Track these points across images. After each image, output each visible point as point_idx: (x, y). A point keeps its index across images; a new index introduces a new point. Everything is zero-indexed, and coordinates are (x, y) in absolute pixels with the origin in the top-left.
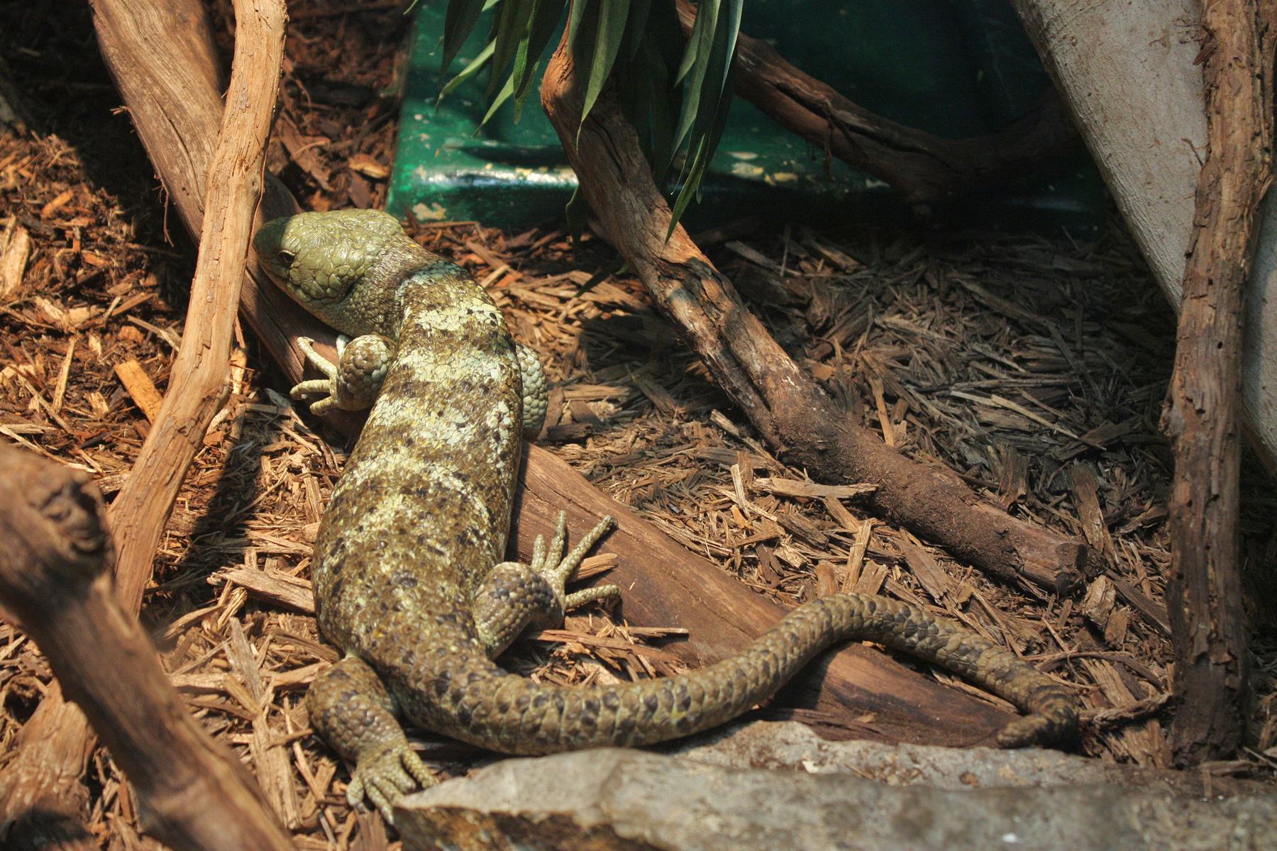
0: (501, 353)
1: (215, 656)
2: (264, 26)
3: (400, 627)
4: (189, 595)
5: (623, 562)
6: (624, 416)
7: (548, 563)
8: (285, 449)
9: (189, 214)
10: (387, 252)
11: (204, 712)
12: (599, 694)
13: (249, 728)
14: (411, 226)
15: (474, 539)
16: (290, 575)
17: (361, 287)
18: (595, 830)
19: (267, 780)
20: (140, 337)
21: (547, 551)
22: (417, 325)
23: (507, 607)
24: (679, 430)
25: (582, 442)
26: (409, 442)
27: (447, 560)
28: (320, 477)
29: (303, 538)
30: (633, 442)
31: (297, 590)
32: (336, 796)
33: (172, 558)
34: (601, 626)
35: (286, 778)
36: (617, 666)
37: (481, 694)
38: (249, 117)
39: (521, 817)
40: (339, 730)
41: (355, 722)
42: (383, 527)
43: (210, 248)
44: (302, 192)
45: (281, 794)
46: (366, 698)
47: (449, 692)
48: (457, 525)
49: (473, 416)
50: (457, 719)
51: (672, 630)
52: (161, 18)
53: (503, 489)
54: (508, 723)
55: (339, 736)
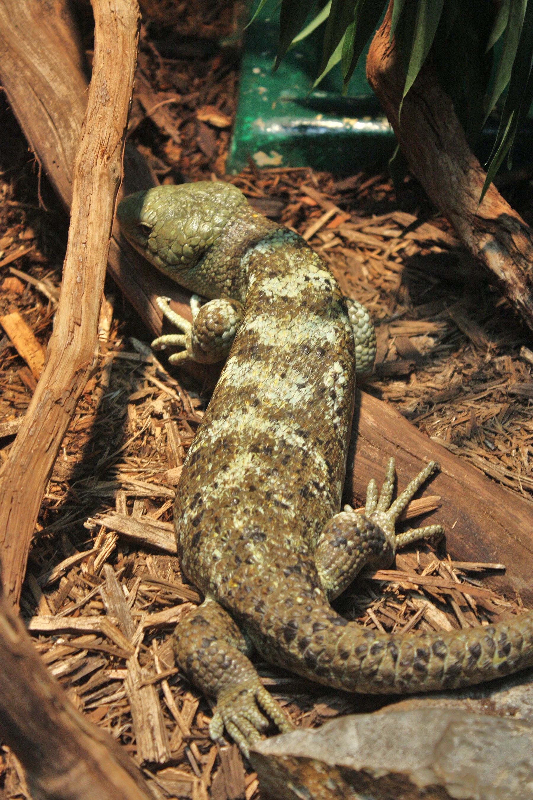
0: (335, 317)
1: (93, 599)
2: (120, 27)
3: (252, 579)
4: (69, 535)
5: (446, 503)
6: (443, 350)
7: (380, 506)
8: (148, 396)
9: (60, 184)
10: (233, 223)
11: (84, 654)
12: (429, 643)
13: (122, 664)
14: (251, 173)
15: (315, 492)
16: (153, 518)
17: (210, 255)
18: (429, 789)
19: (140, 718)
20: (21, 287)
21: (379, 494)
22: (261, 292)
23: (346, 554)
24: (492, 364)
25: (406, 378)
26: (256, 403)
27: (291, 514)
28: (178, 421)
29: (164, 482)
30: (452, 376)
31: (162, 533)
32: (201, 730)
33: (54, 502)
34: (428, 562)
35: (156, 715)
36: (442, 600)
37: (324, 643)
38: (109, 110)
39: (363, 772)
40: (201, 672)
41: (215, 665)
42: (235, 485)
43: (78, 233)
44: (157, 141)
45: (152, 731)
46: (223, 642)
47: (296, 639)
48: (299, 479)
49: (312, 376)
50: (304, 662)
51: (491, 565)
52: (29, 7)
53: (340, 442)
54: (349, 668)
55: (200, 677)
